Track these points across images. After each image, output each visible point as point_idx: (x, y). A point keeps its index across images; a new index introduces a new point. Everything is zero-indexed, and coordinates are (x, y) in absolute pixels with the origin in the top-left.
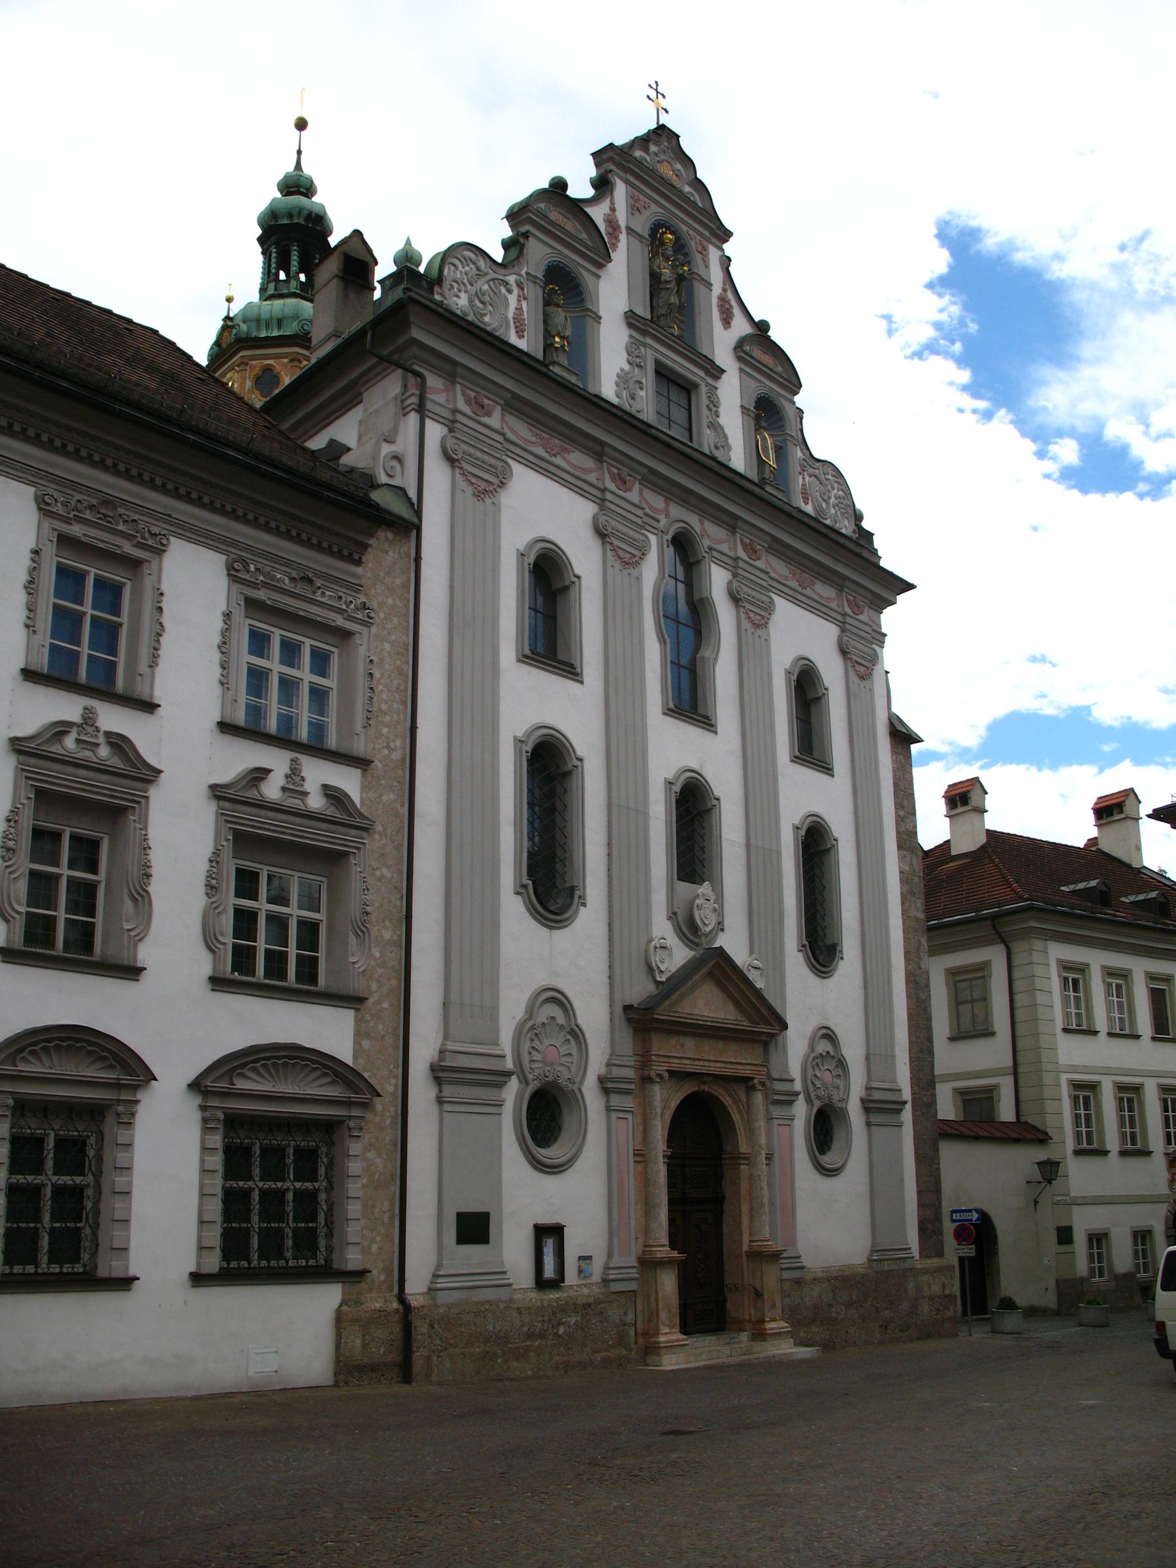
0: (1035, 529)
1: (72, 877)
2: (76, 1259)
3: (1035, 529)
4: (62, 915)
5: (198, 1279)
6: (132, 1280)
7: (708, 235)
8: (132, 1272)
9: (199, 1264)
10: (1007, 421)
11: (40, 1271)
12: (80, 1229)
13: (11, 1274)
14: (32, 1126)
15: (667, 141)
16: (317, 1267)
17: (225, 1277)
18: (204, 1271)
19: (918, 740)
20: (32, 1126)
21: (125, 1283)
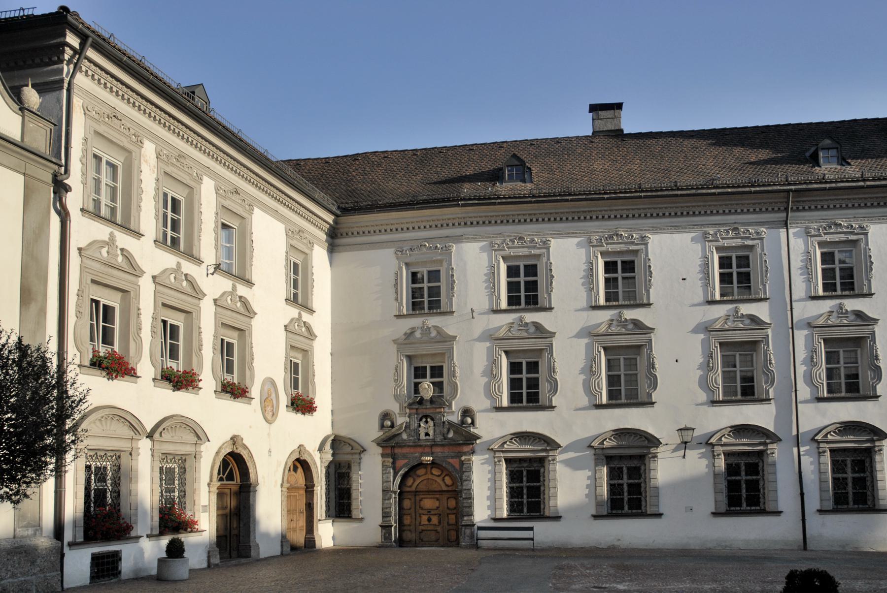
0: (677, 361)
1: (534, 373)
2: (640, 508)
3: (677, 361)
4: (622, 372)
5: (715, 514)
6: (781, 512)
7: (604, 196)
8: (661, 511)
9: (821, 506)
10: (37, 490)
11: (742, 509)
12: (866, 493)
13: (730, 510)
14: (615, 464)
15: (43, 439)
16: (761, 510)
17: (728, 514)
18: (823, 509)
19: (478, 438)
20: (615, 464)
21: (778, 513)
